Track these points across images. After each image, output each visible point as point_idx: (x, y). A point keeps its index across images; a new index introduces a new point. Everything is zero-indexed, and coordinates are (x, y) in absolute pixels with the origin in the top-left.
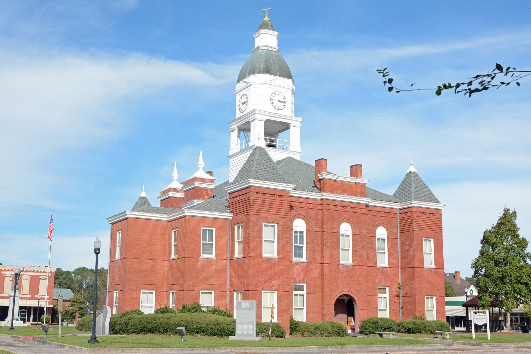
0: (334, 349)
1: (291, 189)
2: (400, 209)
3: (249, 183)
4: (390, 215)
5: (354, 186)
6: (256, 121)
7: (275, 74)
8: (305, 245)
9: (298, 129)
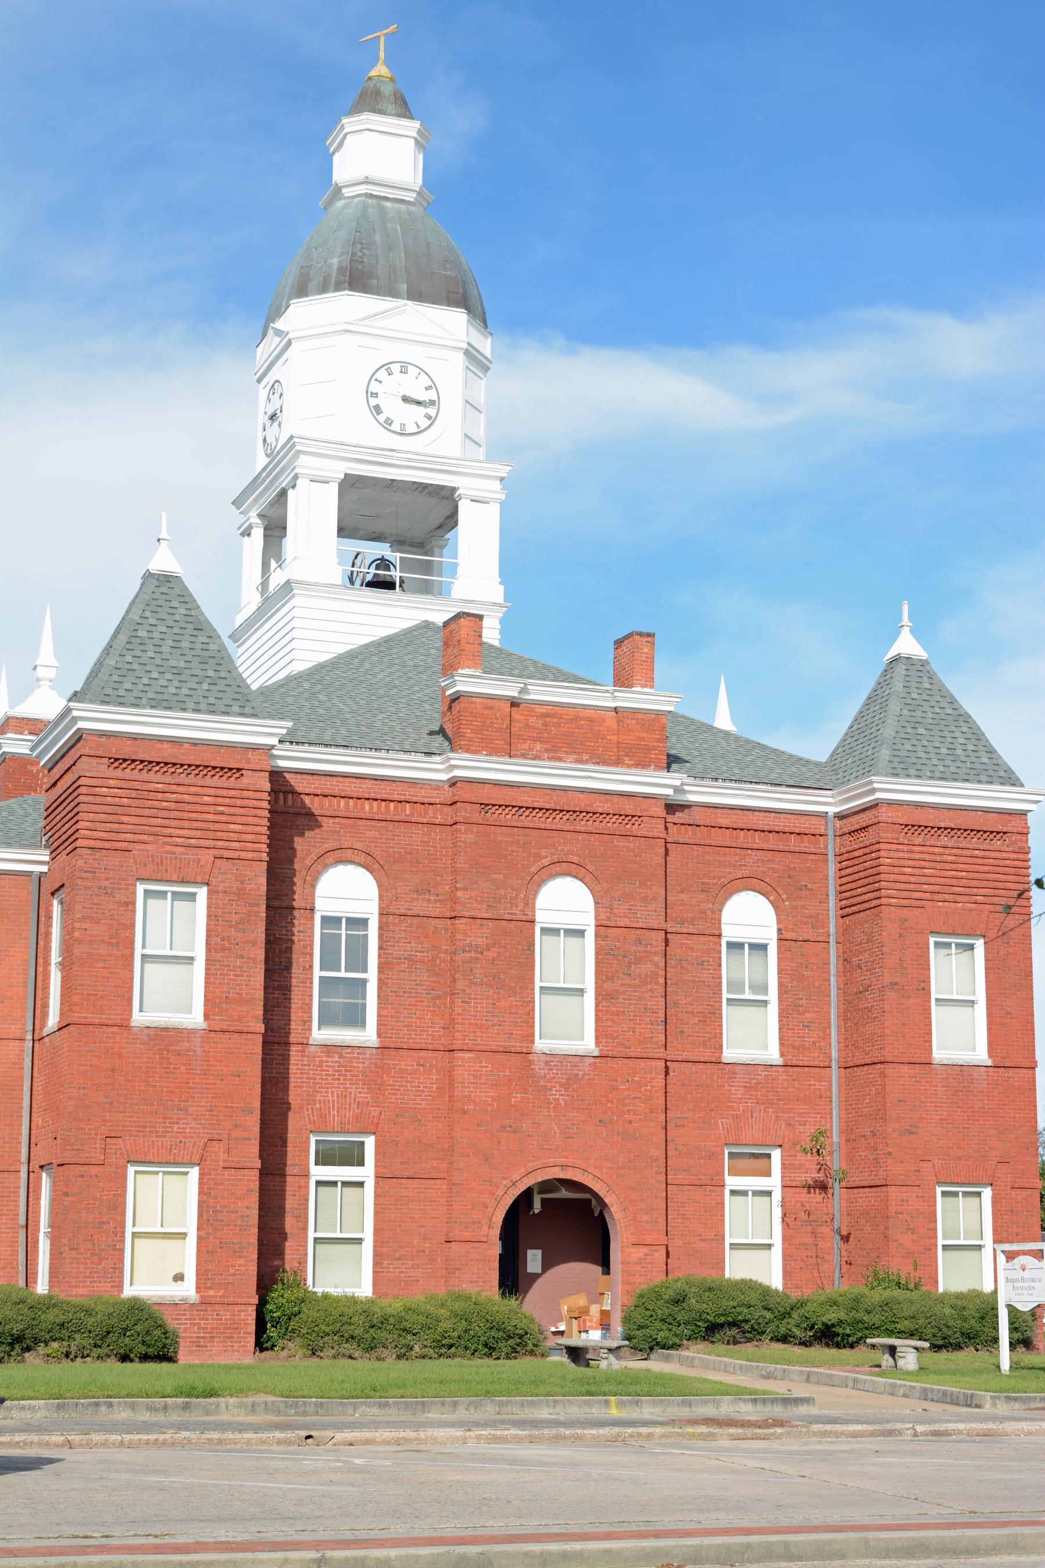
0: (144, 1416)
1: (274, 741)
2: (841, 817)
3: (874, 791)
4: (793, 842)
5: (611, 720)
6: (299, 482)
7: (392, 293)
8: (372, 975)
9: (492, 514)
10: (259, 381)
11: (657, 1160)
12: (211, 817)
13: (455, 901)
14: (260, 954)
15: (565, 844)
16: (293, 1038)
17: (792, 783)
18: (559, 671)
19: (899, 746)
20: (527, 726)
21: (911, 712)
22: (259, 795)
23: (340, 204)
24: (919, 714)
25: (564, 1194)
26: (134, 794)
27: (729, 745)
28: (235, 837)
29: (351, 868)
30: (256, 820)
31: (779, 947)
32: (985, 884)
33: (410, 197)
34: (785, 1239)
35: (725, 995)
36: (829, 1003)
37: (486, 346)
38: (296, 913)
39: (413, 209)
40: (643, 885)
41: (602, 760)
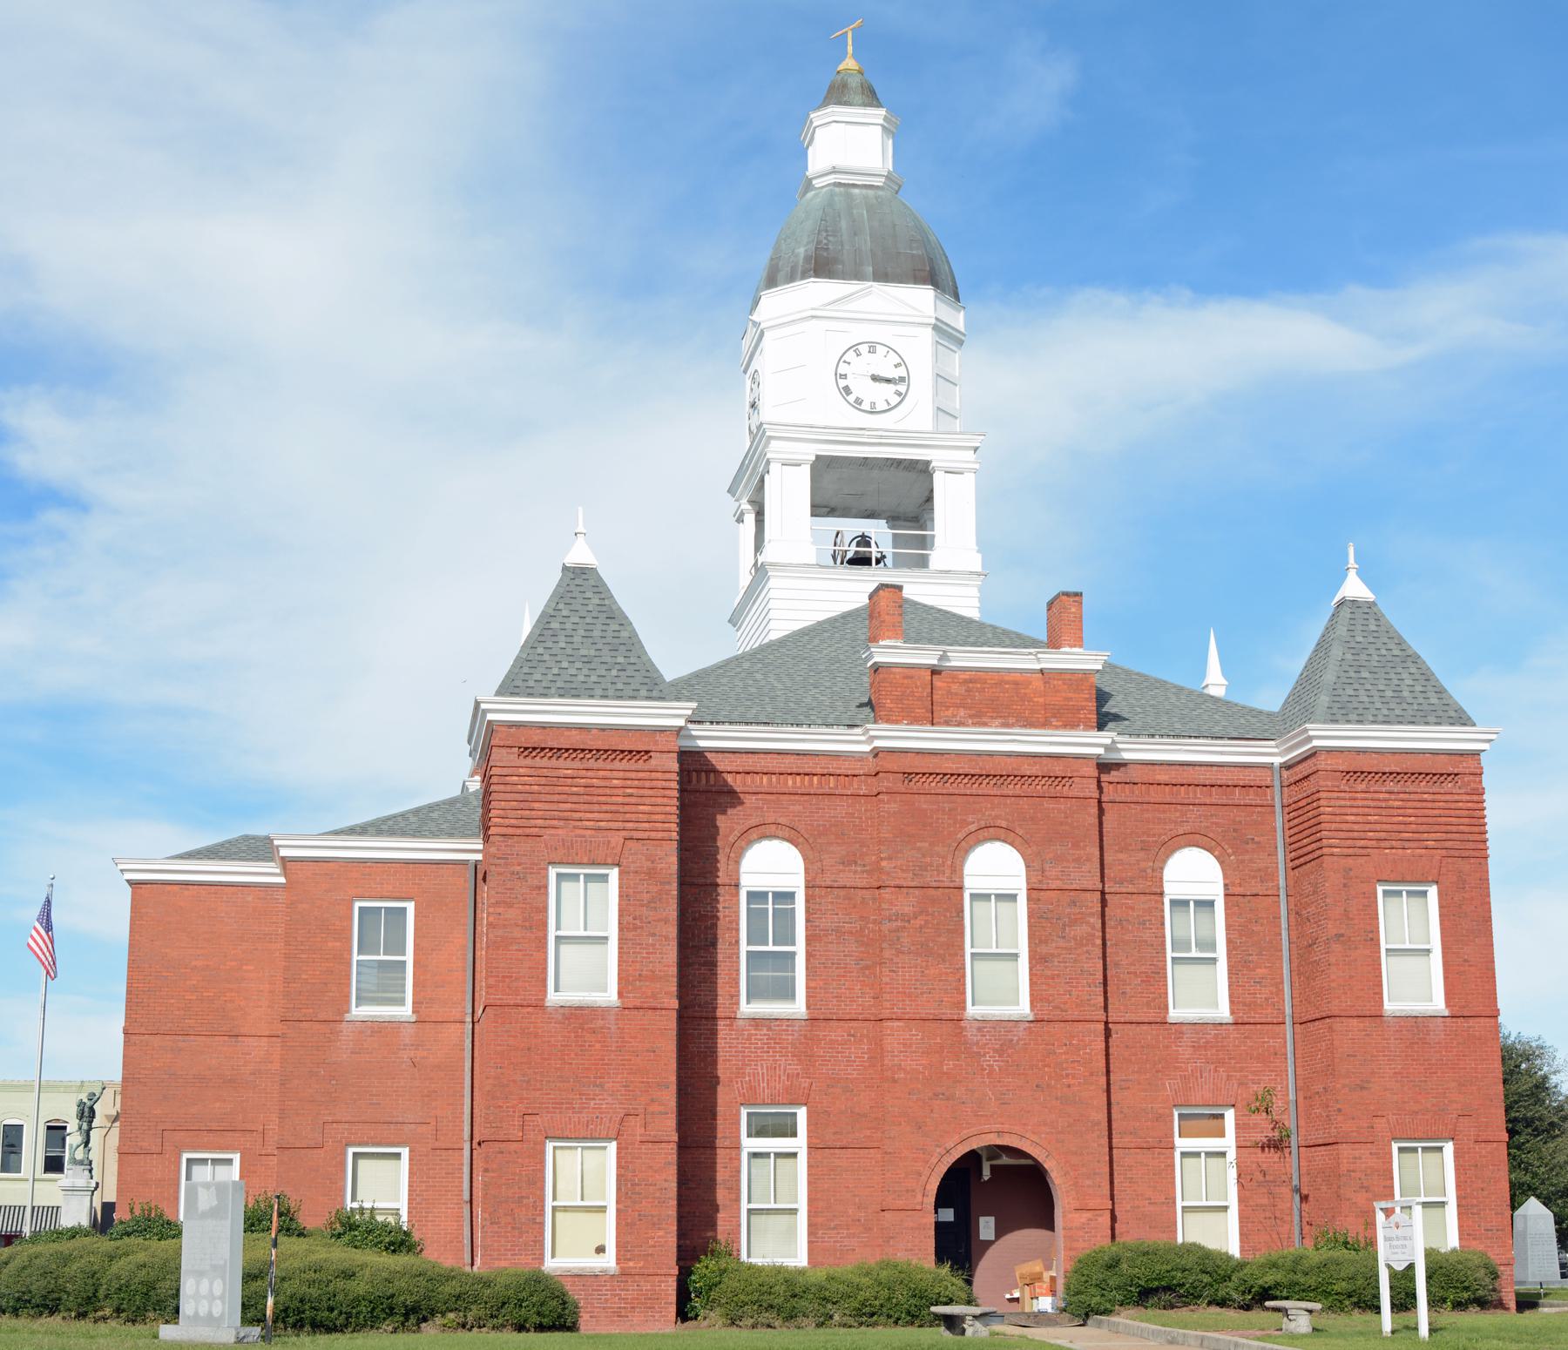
1: (681, 722)
2: (1287, 766)
3: (1310, 739)
5: (1038, 683)
6: (772, 467)
7: (857, 276)
8: (800, 948)
10: (745, 372)
11: (1098, 1123)
12: (620, 800)
13: (881, 870)
14: (672, 931)
15: (992, 809)
16: (719, 1013)
17: (1235, 734)
18: (1018, 635)
19: (1340, 692)
20: (949, 692)
21: (1368, 661)
22: (668, 776)
23: (810, 195)
24: (1363, 657)
25: (1005, 1160)
26: (543, 781)
27: (1179, 699)
28: (645, 817)
29: (776, 843)
30: (665, 801)
31: (1226, 903)
32: (1437, 828)
33: (879, 182)
34: (1241, 1200)
35: (1169, 954)
36: (1281, 958)
37: (958, 320)
38: (721, 890)
39: (881, 193)
40: (1076, 845)
41: (1030, 724)
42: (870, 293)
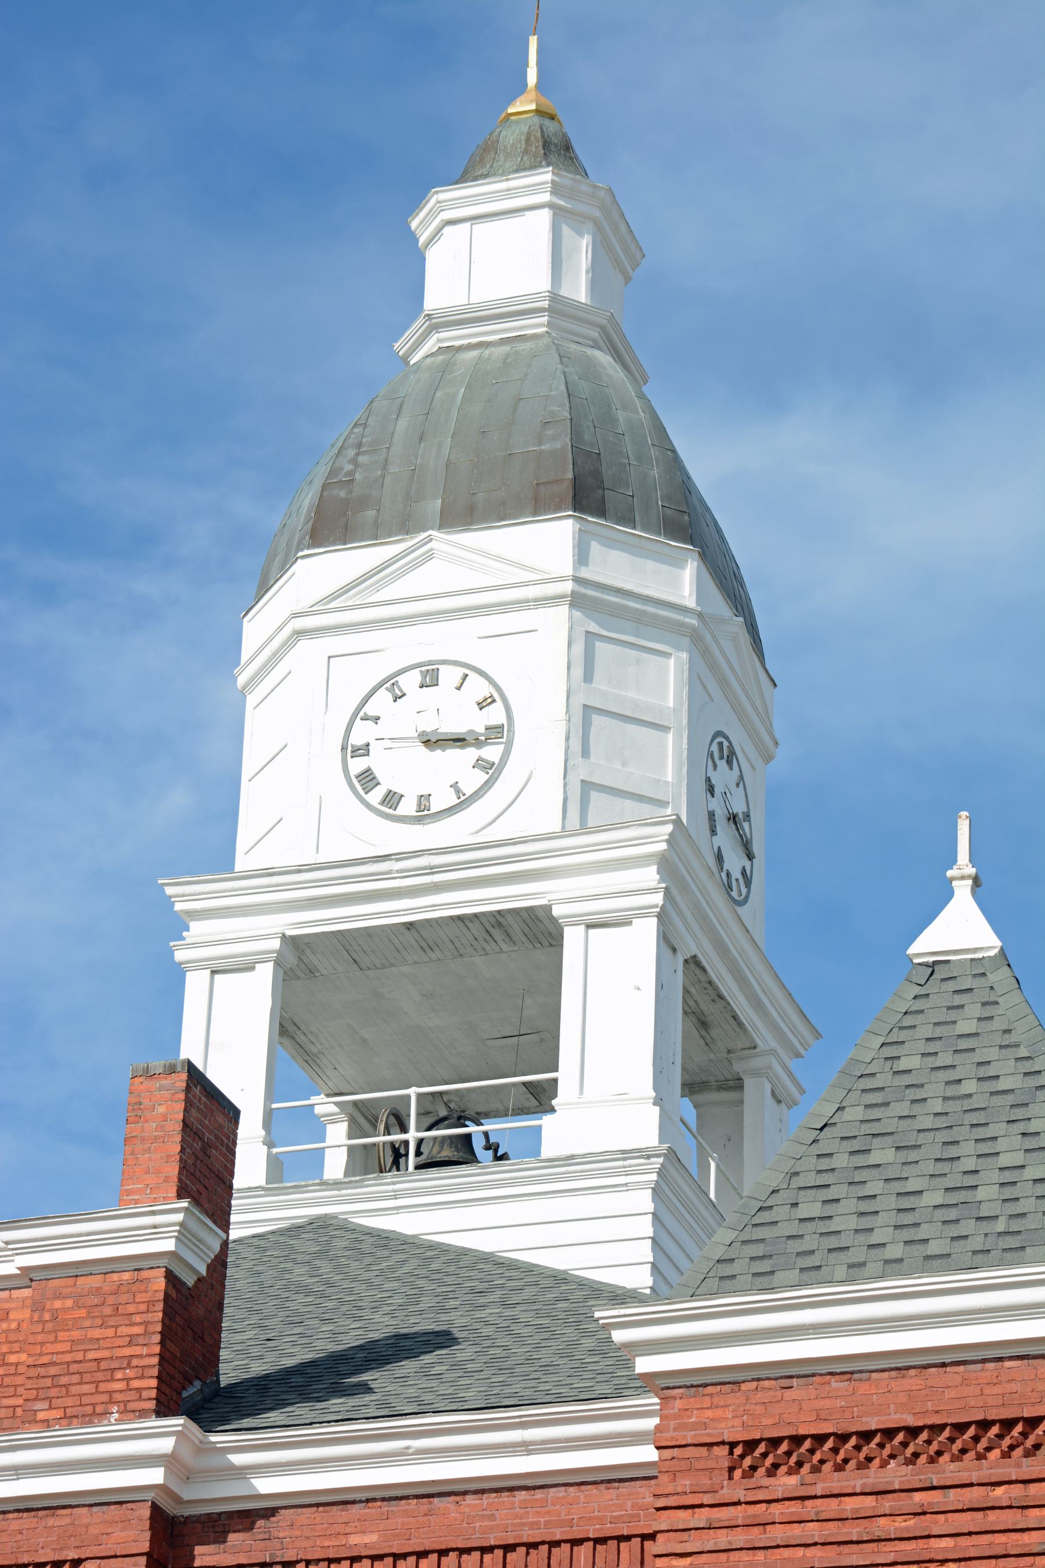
7: (406, 525)
42: (429, 556)
